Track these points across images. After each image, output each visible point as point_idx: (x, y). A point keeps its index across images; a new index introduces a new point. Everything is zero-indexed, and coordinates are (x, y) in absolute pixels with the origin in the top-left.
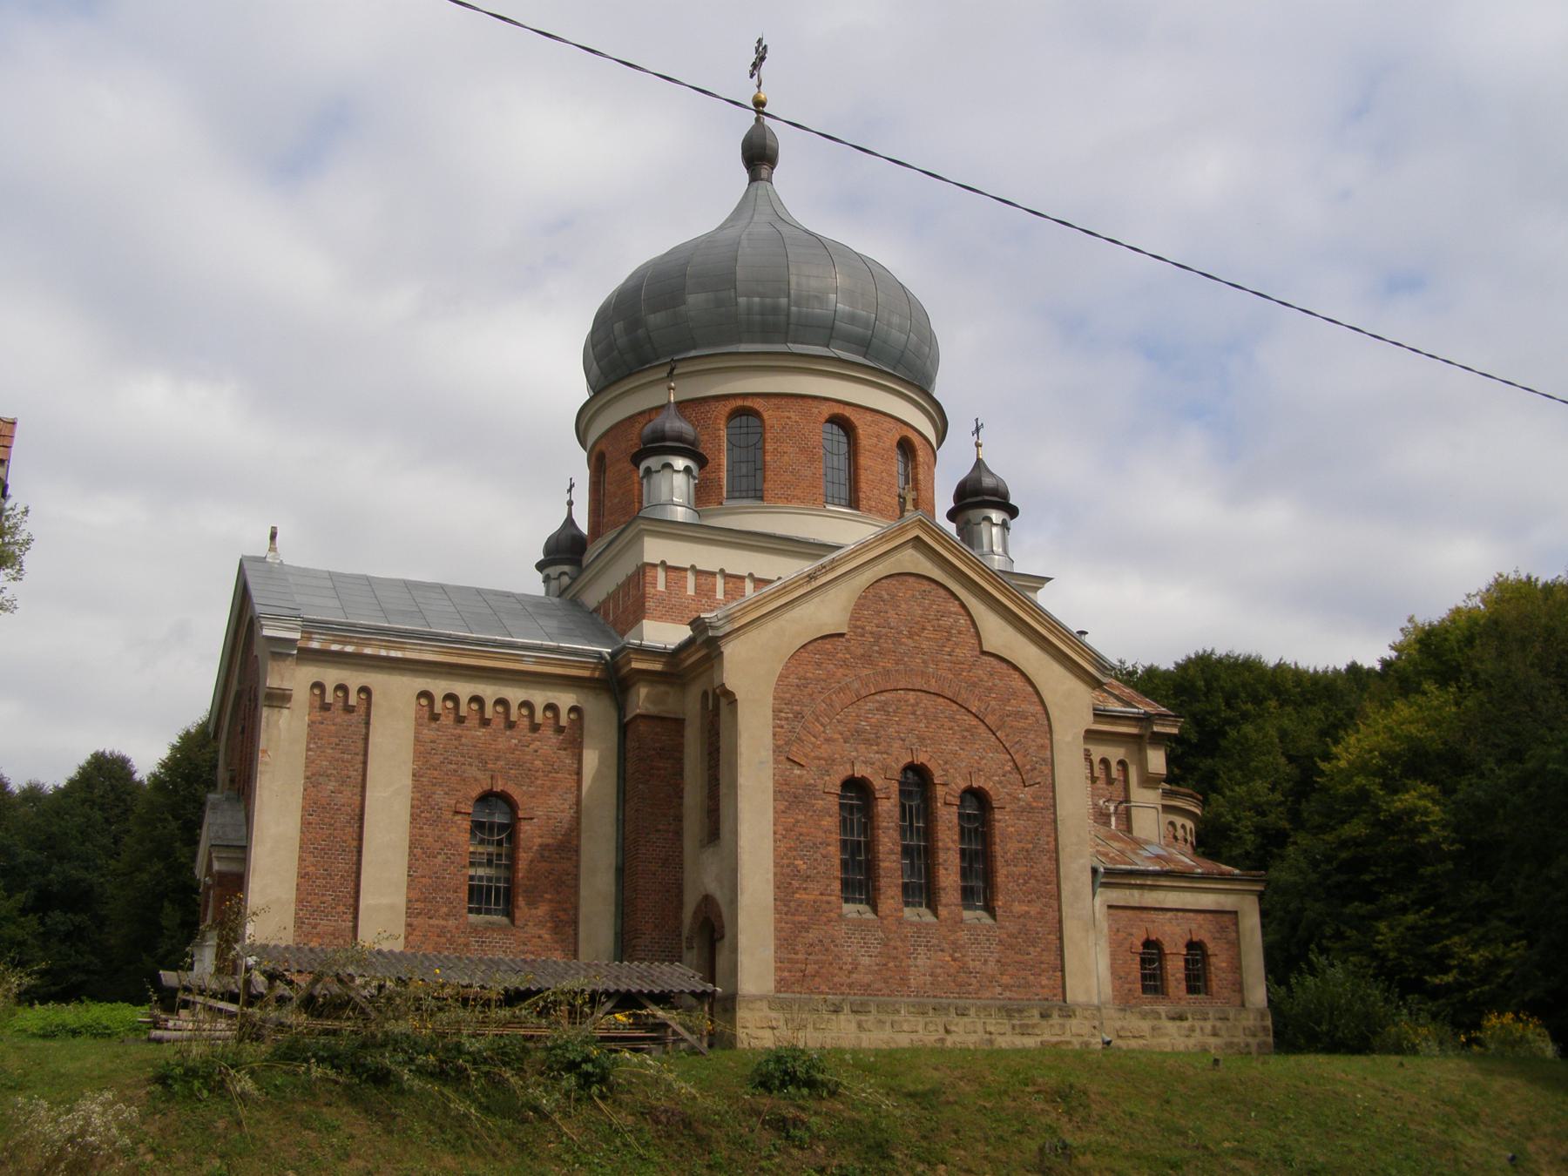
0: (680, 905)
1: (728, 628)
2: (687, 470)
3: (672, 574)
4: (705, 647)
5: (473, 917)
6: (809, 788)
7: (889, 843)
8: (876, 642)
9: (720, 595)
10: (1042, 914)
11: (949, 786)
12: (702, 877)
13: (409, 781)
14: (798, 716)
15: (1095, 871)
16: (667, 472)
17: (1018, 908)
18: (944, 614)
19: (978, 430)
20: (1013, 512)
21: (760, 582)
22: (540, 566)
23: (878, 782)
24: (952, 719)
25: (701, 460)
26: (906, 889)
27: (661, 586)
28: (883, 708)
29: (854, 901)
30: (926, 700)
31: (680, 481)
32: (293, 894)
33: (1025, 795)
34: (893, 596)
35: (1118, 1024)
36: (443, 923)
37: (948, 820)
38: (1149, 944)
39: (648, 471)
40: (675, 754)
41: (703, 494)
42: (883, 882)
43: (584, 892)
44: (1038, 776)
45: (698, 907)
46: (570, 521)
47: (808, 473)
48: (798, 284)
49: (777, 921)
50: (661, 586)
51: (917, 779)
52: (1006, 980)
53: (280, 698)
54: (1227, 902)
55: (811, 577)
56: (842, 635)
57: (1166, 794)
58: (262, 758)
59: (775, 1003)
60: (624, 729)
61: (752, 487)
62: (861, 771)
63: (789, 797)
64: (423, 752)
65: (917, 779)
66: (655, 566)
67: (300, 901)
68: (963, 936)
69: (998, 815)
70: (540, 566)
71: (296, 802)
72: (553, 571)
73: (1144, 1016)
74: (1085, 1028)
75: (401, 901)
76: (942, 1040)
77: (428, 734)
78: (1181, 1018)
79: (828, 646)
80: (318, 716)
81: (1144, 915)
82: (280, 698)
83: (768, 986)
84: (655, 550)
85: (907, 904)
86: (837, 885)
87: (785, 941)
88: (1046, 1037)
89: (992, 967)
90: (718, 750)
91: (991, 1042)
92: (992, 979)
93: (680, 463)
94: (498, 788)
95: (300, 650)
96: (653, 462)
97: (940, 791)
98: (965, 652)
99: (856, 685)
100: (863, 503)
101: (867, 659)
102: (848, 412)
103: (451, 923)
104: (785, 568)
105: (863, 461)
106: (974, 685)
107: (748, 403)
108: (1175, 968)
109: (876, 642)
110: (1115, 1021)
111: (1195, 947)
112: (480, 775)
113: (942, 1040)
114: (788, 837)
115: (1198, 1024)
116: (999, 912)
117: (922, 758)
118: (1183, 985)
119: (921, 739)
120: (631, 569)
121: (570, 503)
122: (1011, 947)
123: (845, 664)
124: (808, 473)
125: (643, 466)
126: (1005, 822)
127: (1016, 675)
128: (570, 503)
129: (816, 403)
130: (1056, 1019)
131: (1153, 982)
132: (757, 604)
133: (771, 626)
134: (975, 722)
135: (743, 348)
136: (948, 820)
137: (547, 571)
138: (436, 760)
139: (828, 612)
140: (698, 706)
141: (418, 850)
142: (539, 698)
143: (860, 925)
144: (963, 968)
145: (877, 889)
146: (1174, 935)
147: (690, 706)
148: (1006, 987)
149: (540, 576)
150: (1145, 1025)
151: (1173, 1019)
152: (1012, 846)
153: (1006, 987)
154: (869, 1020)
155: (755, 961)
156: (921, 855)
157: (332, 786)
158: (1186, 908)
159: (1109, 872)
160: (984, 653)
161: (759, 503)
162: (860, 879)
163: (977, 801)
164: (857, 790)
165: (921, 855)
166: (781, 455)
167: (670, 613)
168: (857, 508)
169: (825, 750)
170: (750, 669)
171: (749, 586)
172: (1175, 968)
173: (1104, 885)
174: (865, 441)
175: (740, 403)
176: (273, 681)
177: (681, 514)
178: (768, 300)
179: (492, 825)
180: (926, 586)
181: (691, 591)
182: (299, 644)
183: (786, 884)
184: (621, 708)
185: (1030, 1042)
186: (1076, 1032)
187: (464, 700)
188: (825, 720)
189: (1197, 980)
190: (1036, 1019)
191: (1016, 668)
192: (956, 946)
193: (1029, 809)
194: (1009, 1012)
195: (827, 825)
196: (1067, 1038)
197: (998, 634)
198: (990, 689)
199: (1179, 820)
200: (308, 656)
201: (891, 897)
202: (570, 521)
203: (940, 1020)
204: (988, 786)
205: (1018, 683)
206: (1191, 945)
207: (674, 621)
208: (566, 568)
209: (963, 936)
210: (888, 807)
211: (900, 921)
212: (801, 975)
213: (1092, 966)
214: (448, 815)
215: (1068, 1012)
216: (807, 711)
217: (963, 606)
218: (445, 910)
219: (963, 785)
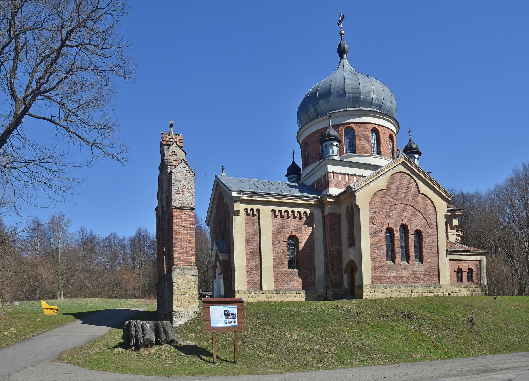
0: (342, 263)
1: (357, 189)
3: (342, 175)
4: (349, 193)
6: (378, 231)
7: (398, 245)
9: (355, 181)
10: (434, 262)
11: (412, 229)
12: (348, 255)
13: (271, 234)
14: (375, 212)
15: (447, 251)
16: (332, 146)
17: (428, 261)
18: (409, 183)
20: (420, 154)
22: (287, 176)
23: (394, 229)
24: (412, 211)
25: (340, 142)
26: (402, 257)
28: (395, 209)
29: (390, 260)
31: (335, 148)
32: (245, 264)
33: (430, 231)
34: (397, 178)
35: (451, 289)
37: (412, 238)
38: (458, 269)
39: (326, 146)
40: (339, 223)
41: (340, 152)
42: (396, 255)
43: (316, 260)
44: (433, 226)
45: (348, 263)
46: (294, 163)
47: (367, 145)
48: (363, 89)
49: (372, 266)
50: (332, 178)
51: (404, 228)
52: (426, 279)
53: (237, 213)
54: (478, 258)
55: (377, 174)
56: (385, 190)
57: (457, 231)
58: (234, 229)
59: (372, 286)
60: (324, 218)
61: (353, 150)
63: (374, 234)
64: (274, 226)
67: (248, 266)
68: (415, 268)
69: (424, 237)
70: (287, 176)
71: (244, 240)
72: (290, 176)
73: (457, 287)
74: (444, 291)
75: (272, 265)
76: (411, 295)
77: (275, 220)
79: (381, 192)
80: (247, 217)
81: (458, 262)
82: (237, 213)
83: (370, 282)
84: (331, 168)
85: (402, 260)
86: (385, 256)
87: (374, 271)
88: (435, 293)
89: (422, 276)
90: (353, 222)
91: (422, 295)
92: (422, 279)
93: (335, 143)
94: (293, 235)
95: (242, 199)
96: (328, 143)
97: (410, 231)
98: (416, 193)
100: (382, 153)
101: (391, 196)
102: (377, 127)
103: (284, 270)
104: (367, 173)
105: (381, 141)
106: (418, 202)
108: (465, 275)
110: (450, 289)
111: (470, 270)
112: (288, 231)
113: (411, 295)
114: (374, 244)
116: (424, 262)
117: (405, 222)
118: (467, 280)
119: (405, 217)
120: (323, 174)
121: (293, 157)
122: (427, 271)
123: (386, 197)
124: (367, 145)
125: (324, 145)
126: (426, 239)
128: (293, 157)
129: (369, 125)
130: (438, 289)
131: (460, 279)
132: (364, 182)
133: (367, 187)
134: (418, 212)
135: (348, 109)
136: (412, 238)
137: (289, 176)
138: (277, 228)
139: (381, 183)
140: (346, 210)
141: (275, 252)
142: (302, 210)
143: (392, 267)
144: (416, 277)
145: (395, 257)
146: (465, 266)
147: (343, 210)
148: (425, 281)
149: (287, 178)
150: (458, 290)
152: (427, 245)
153: (425, 281)
154: (394, 290)
155: (367, 277)
156: (406, 247)
157: (252, 236)
158: (469, 260)
159: (451, 251)
160: (420, 193)
163: (418, 233)
164: (390, 231)
165: (406, 247)
166: (359, 139)
167: (336, 186)
168: (380, 155)
170: (363, 199)
172: (465, 275)
173: (449, 254)
174: (382, 135)
176: (235, 208)
177: (336, 158)
179: (292, 244)
180: (405, 175)
181: (340, 179)
182: (241, 198)
183: (374, 256)
184: (323, 213)
185: (431, 295)
186: (442, 292)
187: (283, 212)
188: (381, 213)
189: (470, 278)
190: (433, 289)
192: (414, 271)
193: (431, 235)
194: (427, 287)
195: (383, 241)
196: (440, 293)
199: (458, 238)
200: (244, 202)
201: (398, 259)
202: (294, 163)
203: (411, 289)
205: (429, 201)
206: (469, 269)
207: (336, 188)
208: (294, 175)
209: (415, 268)
210: (397, 235)
211: (400, 265)
212: (376, 280)
213: (446, 275)
214: (281, 242)
215: (440, 287)
216: (377, 211)
219: (415, 229)
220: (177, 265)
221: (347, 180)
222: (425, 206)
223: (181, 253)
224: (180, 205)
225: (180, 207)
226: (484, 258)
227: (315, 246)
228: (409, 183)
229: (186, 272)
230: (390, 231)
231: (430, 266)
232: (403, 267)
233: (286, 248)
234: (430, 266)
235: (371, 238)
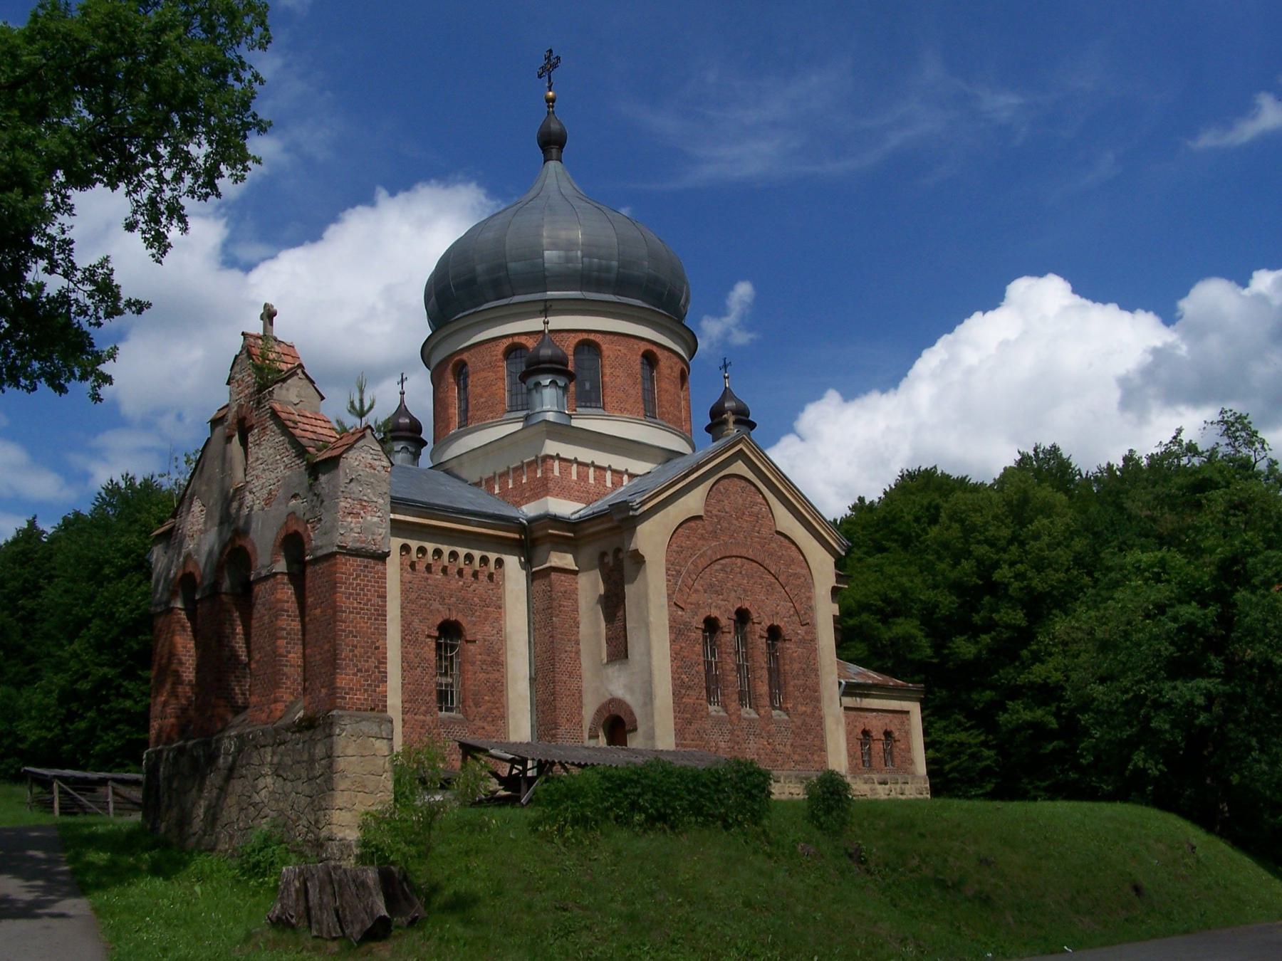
2: (553, 383)
3: (563, 464)
5: (443, 714)
6: (685, 624)
8: (719, 523)
9: (609, 484)
17: (801, 709)
18: (756, 504)
19: (402, 381)
21: (632, 476)
24: (761, 578)
27: (557, 473)
30: (748, 565)
36: (422, 717)
50: (557, 473)
51: (742, 617)
52: (796, 757)
56: (700, 517)
62: (715, 613)
63: (678, 631)
65: (742, 617)
66: (551, 457)
68: (773, 727)
78: (885, 783)
80: (408, 576)
89: (788, 750)
92: (789, 756)
99: (709, 552)
102: (655, 349)
103: (428, 718)
106: (772, 554)
107: (592, 337)
109: (719, 523)
115: (893, 786)
117: (747, 605)
119: (745, 591)
121: (402, 393)
123: (702, 538)
127: (794, 548)
128: (402, 393)
134: (773, 580)
138: (413, 596)
148: (797, 763)
151: (880, 783)
153: (797, 763)
161: (601, 411)
162: (713, 685)
164: (711, 625)
169: (694, 598)
171: (625, 478)
175: (585, 336)
178: (604, 262)
180: (744, 484)
181: (574, 477)
191: (794, 543)
197: (785, 521)
198: (780, 557)
204: (782, 625)
205: (795, 553)
207: (565, 498)
209: (773, 727)
214: (422, 638)
217: (764, 497)
218: (424, 708)
220: (343, 708)
221: (591, 481)
222: (788, 566)
223: (355, 674)
224: (358, 545)
225: (357, 550)
226: (915, 708)
227: (509, 653)
228: (756, 504)
229: (365, 727)
230: (711, 625)
231: (804, 724)
232: (745, 724)
233: (432, 655)
234: (804, 724)
235: (673, 642)
